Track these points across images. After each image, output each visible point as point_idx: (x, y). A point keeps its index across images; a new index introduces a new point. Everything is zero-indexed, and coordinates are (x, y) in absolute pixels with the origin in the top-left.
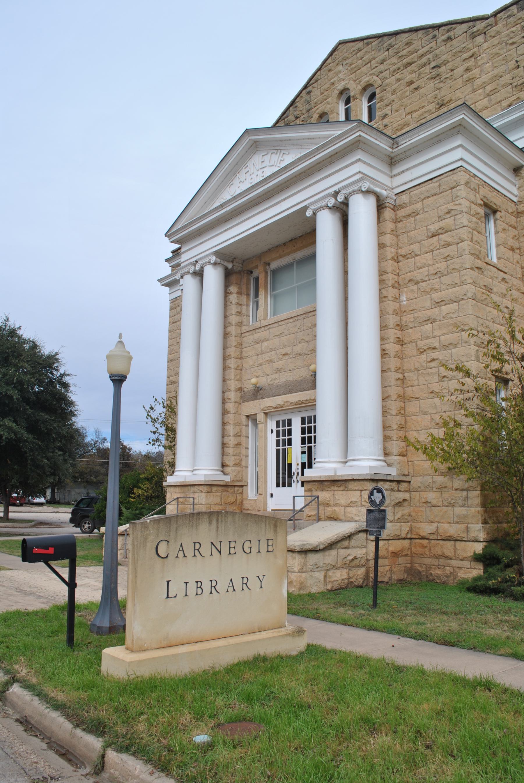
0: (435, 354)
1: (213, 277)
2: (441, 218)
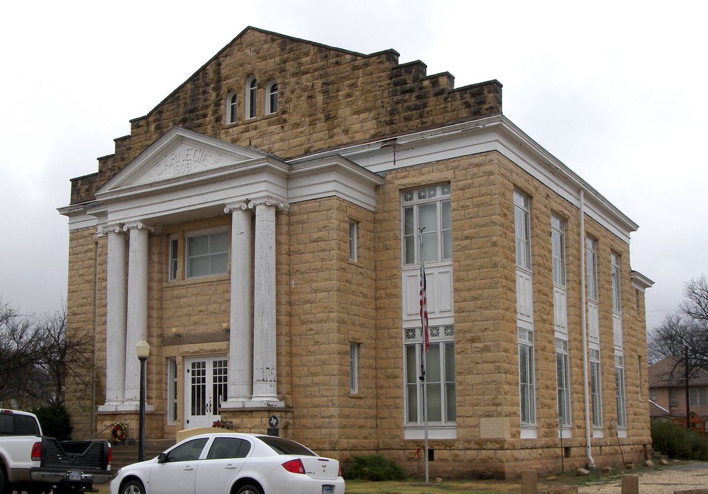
0: (312, 326)
1: (138, 241)
2: (320, 230)
